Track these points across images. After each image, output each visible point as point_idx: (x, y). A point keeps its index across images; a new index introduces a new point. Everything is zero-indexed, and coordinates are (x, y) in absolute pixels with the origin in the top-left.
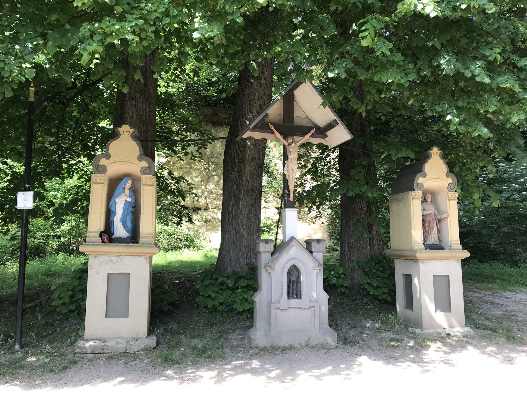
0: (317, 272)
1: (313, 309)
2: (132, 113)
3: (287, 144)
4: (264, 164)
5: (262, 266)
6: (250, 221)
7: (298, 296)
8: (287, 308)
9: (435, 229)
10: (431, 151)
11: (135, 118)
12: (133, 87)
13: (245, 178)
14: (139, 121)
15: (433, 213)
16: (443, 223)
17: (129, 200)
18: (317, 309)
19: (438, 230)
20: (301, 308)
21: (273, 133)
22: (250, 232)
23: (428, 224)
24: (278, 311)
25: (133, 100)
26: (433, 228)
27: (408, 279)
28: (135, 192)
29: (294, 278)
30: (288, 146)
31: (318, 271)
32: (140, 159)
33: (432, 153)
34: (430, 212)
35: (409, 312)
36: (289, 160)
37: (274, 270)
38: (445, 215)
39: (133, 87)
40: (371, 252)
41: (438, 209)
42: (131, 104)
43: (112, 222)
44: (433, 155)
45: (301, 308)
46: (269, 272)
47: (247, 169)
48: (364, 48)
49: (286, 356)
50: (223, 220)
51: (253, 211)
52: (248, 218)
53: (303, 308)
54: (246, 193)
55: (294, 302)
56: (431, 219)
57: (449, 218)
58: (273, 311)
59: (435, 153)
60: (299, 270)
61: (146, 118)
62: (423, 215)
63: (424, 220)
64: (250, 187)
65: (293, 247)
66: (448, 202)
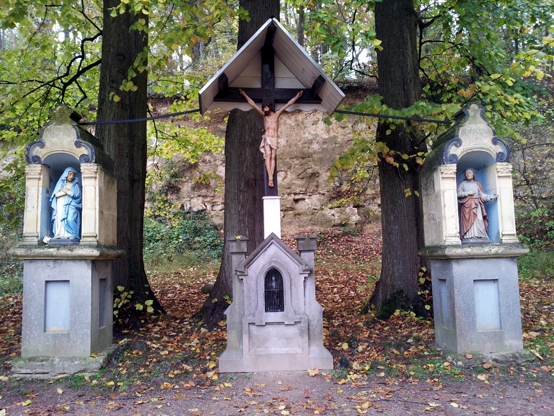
0: (305, 278)
1: (299, 325)
3: (264, 114)
4: (379, 169)
8: (264, 324)
9: (480, 217)
10: (468, 110)
19: (485, 218)
20: (282, 323)
23: (469, 209)
24: (253, 328)
26: (475, 215)
30: (265, 116)
31: (307, 275)
34: (471, 192)
37: (247, 275)
45: (282, 323)
46: (240, 277)
49: (57, 265)
50: (144, 201)
53: (286, 323)
55: (273, 316)
62: (460, 198)
63: (461, 206)
65: (272, 245)
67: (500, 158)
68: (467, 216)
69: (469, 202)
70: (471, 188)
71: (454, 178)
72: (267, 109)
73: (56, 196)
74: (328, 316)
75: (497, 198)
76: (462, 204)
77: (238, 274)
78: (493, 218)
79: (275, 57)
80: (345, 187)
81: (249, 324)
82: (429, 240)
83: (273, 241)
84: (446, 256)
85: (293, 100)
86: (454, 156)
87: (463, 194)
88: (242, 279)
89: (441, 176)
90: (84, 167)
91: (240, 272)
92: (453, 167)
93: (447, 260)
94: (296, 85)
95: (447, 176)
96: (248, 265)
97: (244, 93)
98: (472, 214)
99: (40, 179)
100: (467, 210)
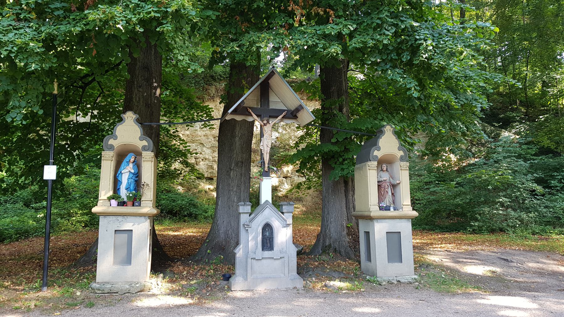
1: (283, 259)
2: (139, 98)
5: (242, 225)
6: (240, 189)
7: (271, 248)
9: (390, 193)
11: (141, 102)
12: (140, 76)
13: (235, 152)
14: (145, 105)
15: (388, 181)
16: (397, 189)
17: (133, 171)
18: (286, 259)
19: (393, 194)
20: (272, 258)
21: (252, 116)
22: (240, 197)
25: (140, 87)
26: (387, 192)
27: (367, 234)
28: (138, 165)
29: (267, 234)
32: (141, 139)
33: (386, 130)
34: (385, 179)
35: (369, 263)
36: (265, 136)
38: (398, 182)
39: (140, 76)
40: (347, 214)
41: (392, 177)
42: (138, 91)
43: (119, 189)
44: (386, 131)
45: (272, 258)
46: (246, 229)
47: (237, 144)
48: (52, 161)
51: (242, 180)
52: (238, 186)
54: (237, 164)
55: (267, 254)
56: (386, 186)
57: (401, 184)
58: (249, 260)
59: (388, 130)
60: (272, 228)
61: (151, 102)
62: (378, 182)
63: (379, 186)
64: (240, 159)
66: (400, 171)
67: (402, 159)
68: (383, 193)
69: (384, 184)
70: (385, 176)
71: (375, 170)
72: (265, 122)
73: (122, 172)
74: (299, 253)
75: (400, 183)
76: (380, 185)
77: (245, 226)
78: (397, 195)
79: (270, 91)
80: (320, 211)
81: (252, 258)
82: (358, 206)
83: (268, 206)
84: (370, 216)
85: (281, 117)
86: (376, 156)
87: (380, 179)
88: (247, 230)
89: (143, 160)
90: (144, 153)
91: (247, 225)
92: (376, 163)
93: (370, 219)
94: (282, 107)
95: (147, 160)
96: (251, 221)
97: (251, 111)
98: (385, 192)
99: (112, 160)
100: (383, 189)
